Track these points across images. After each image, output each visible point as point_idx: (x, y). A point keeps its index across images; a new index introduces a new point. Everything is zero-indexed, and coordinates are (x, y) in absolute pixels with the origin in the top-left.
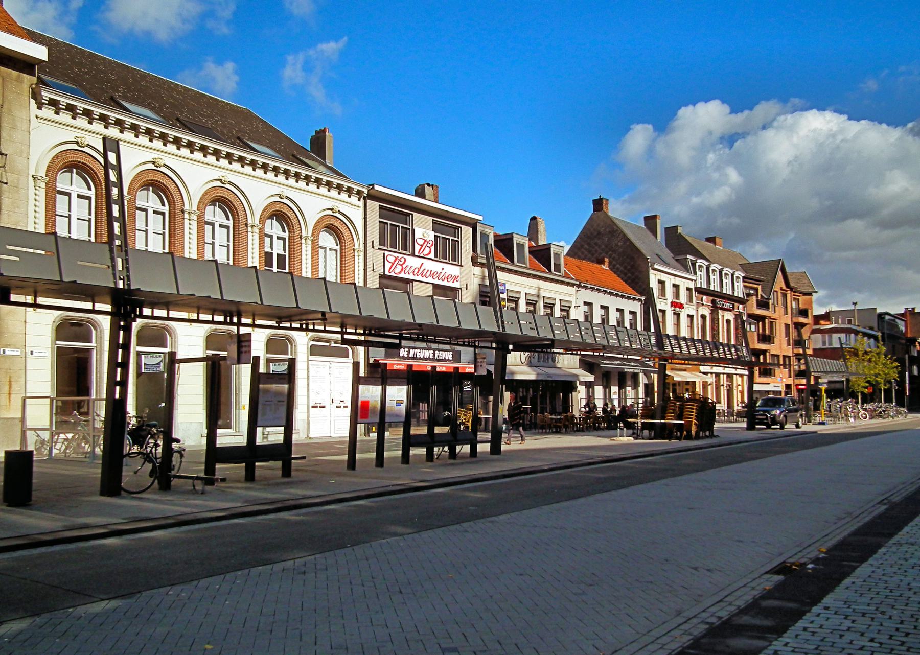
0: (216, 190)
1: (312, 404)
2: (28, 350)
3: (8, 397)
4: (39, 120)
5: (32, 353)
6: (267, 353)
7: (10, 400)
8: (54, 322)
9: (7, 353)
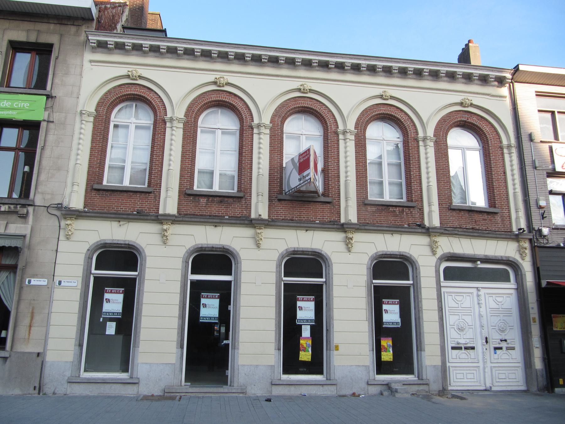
0: (295, 101)
1: (450, 344)
2: (57, 280)
3: (28, 329)
4: (92, 64)
5: (60, 283)
6: (375, 278)
7: (30, 333)
8: (88, 250)
9: (33, 283)
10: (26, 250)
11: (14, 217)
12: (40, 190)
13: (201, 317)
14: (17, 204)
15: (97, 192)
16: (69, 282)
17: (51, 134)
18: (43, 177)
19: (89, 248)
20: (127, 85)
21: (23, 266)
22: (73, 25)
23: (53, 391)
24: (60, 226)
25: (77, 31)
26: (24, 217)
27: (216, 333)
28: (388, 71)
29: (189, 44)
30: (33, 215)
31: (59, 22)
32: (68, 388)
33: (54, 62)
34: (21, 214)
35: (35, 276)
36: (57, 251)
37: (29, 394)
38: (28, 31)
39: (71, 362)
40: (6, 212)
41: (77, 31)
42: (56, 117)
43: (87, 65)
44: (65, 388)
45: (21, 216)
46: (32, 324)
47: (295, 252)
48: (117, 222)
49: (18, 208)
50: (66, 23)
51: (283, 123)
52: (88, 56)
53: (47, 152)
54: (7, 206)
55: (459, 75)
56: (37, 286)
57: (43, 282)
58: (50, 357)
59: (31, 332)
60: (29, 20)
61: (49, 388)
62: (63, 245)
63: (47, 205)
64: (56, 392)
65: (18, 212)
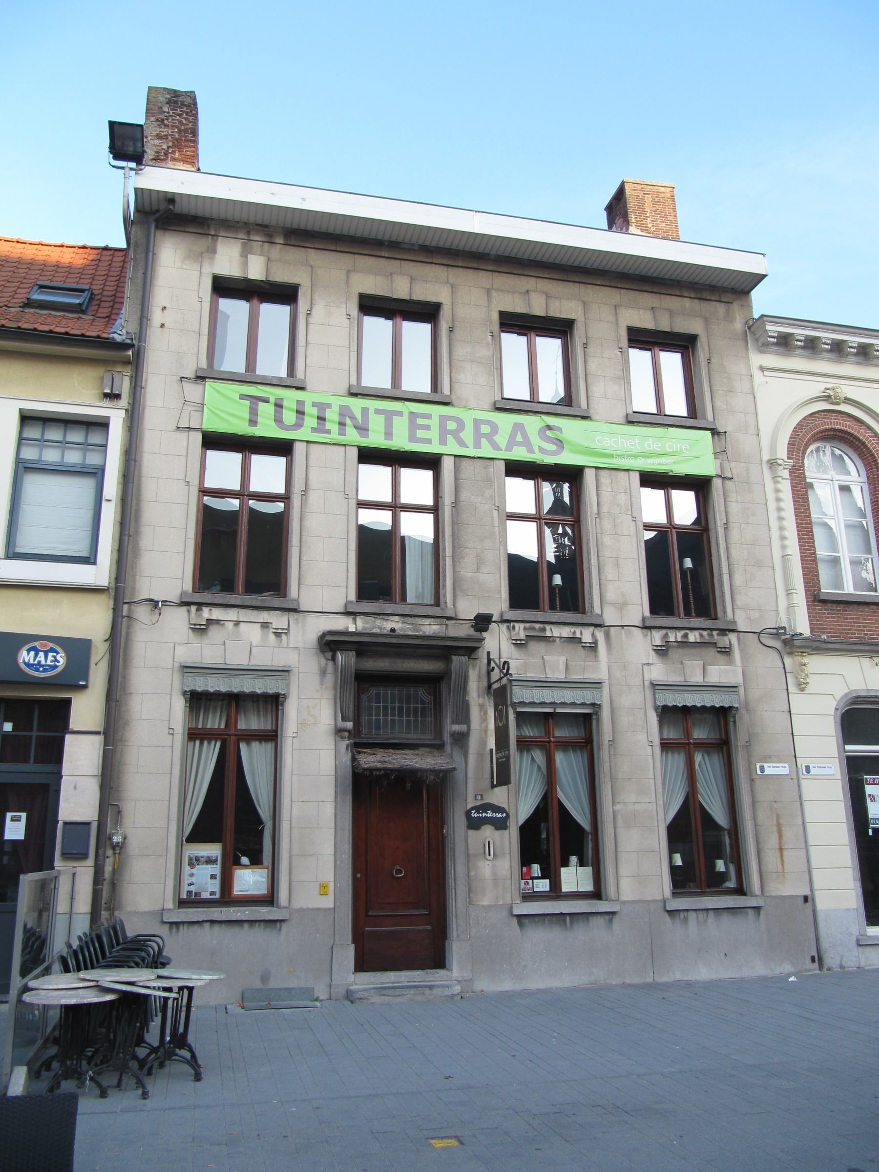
3: (778, 855)
4: (766, 373)
5: (808, 769)
7: (782, 861)
9: (767, 771)
10: (743, 711)
11: (711, 653)
12: (739, 603)
13: (871, 819)
14: (712, 630)
15: (823, 605)
16: (822, 767)
17: (732, 500)
18: (738, 579)
19: (837, 705)
20: (822, 413)
21: (747, 742)
22: (720, 301)
23: (838, 963)
24: (784, 668)
25: (728, 311)
26: (726, 652)
27: (5, 860)
28: (838, 349)
29: (815, 329)
30: (740, 650)
31: (699, 296)
32: (860, 955)
33: (707, 369)
34: (720, 648)
35: (767, 758)
36: (790, 711)
37: (806, 970)
38: (548, 297)
39: (855, 909)
40: (697, 644)
41: (728, 311)
42: (734, 469)
43: (758, 375)
44: (855, 957)
45: (518, 642)
46: (782, 844)
47: (857, 699)
48: (867, 660)
49: (716, 637)
50: (709, 298)
51: (490, 426)
52: (757, 359)
53: (734, 534)
54: (697, 633)
55: (825, 344)
56: (775, 777)
57: (781, 769)
58: (822, 903)
59: (785, 859)
60: (475, 266)
61: (831, 958)
62: (798, 701)
63: (759, 631)
64: (844, 963)
65: (715, 643)
